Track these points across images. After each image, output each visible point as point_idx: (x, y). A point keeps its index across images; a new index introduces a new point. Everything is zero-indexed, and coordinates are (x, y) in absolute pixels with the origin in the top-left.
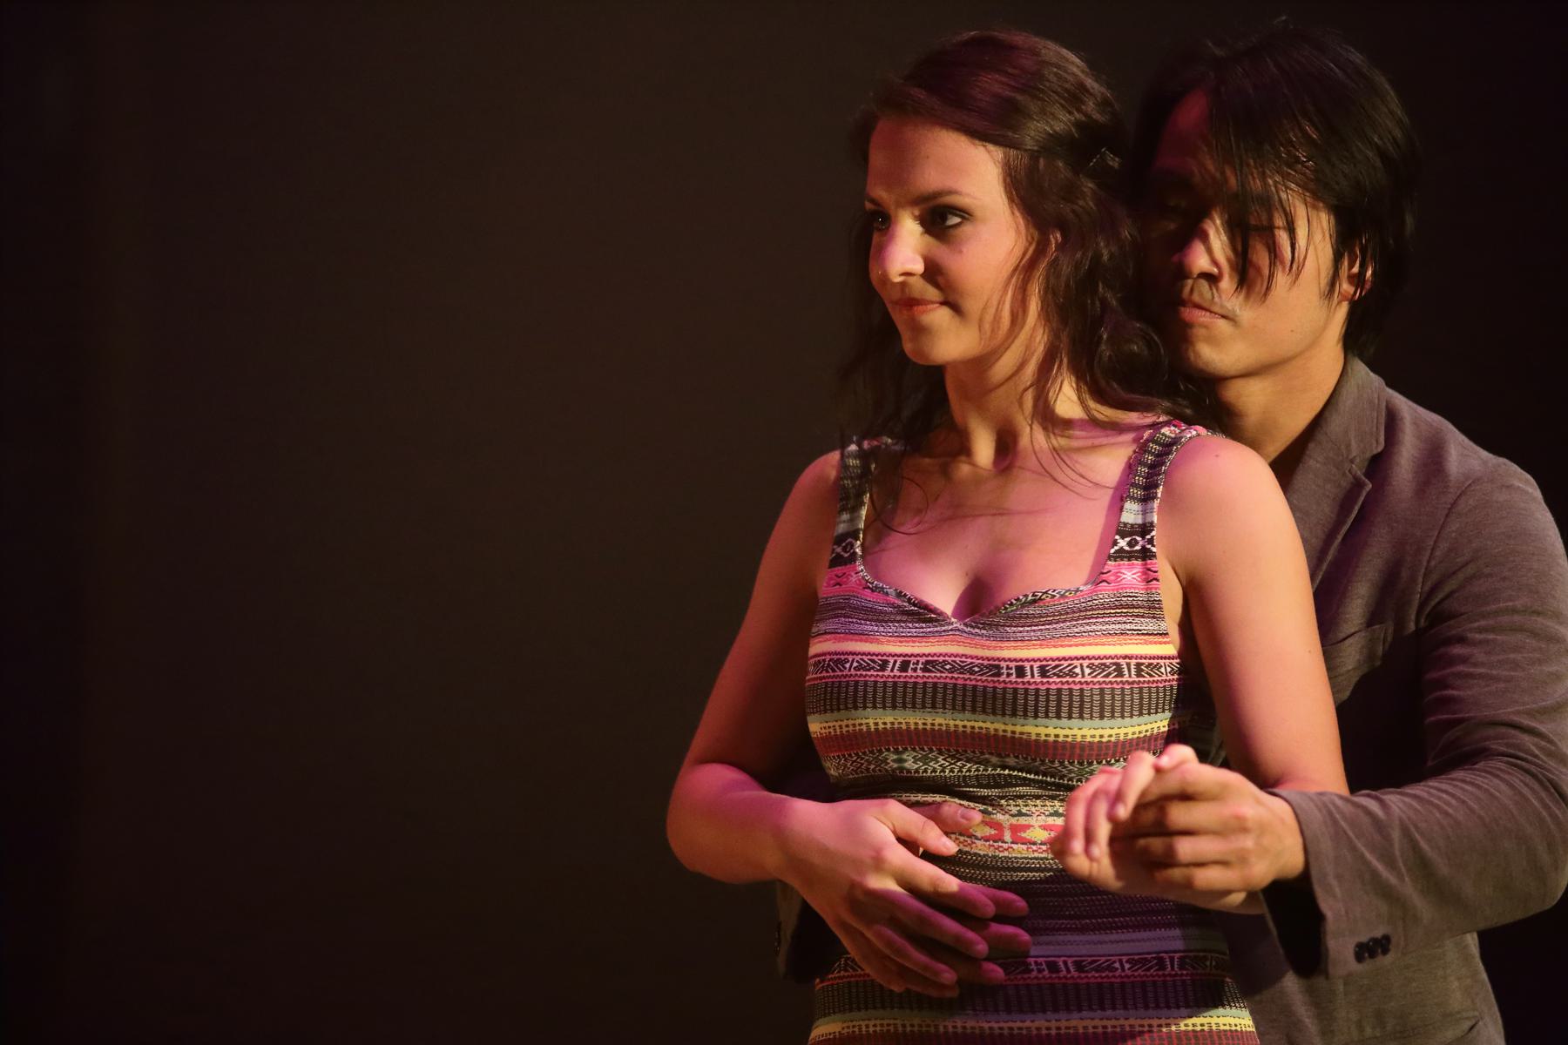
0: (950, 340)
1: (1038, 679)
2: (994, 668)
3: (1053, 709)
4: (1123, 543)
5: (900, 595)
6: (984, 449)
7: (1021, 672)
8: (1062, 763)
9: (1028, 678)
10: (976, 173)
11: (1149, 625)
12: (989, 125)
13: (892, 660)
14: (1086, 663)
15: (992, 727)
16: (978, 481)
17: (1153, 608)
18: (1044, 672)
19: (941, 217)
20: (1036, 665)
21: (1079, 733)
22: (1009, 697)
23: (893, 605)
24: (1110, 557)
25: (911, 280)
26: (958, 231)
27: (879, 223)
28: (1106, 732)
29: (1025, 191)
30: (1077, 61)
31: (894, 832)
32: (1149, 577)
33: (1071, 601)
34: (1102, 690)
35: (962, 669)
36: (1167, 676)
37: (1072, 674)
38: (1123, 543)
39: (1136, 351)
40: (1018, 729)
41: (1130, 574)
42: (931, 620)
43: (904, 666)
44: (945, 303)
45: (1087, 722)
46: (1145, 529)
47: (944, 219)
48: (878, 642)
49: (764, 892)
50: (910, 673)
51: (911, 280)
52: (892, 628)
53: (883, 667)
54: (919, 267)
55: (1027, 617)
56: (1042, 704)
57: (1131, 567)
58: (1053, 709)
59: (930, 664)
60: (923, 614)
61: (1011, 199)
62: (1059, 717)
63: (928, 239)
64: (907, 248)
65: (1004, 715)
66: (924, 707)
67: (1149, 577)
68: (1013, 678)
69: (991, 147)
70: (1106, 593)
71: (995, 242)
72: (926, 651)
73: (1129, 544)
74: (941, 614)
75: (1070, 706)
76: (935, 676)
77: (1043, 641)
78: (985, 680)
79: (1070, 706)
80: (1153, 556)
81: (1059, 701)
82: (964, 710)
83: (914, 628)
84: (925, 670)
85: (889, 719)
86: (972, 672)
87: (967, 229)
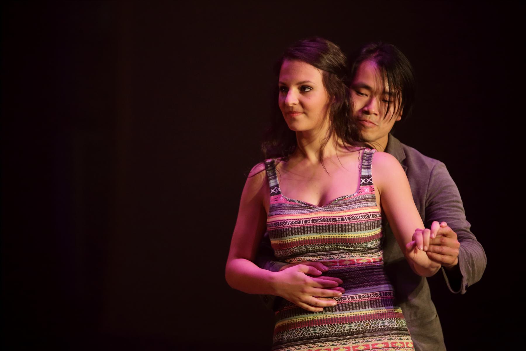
0: (302, 123)
1: (348, 221)
2: (335, 219)
3: (353, 229)
4: (363, 181)
5: (299, 202)
6: (313, 157)
7: (343, 219)
8: (355, 244)
9: (345, 221)
10: (314, 75)
11: (373, 203)
12: (315, 61)
13: (302, 220)
14: (360, 215)
15: (335, 236)
16: (313, 166)
17: (373, 199)
18: (349, 219)
19: (304, 88)
20: (347, 217)
21: (360, 235)
22: (340, 227)
23: (298, 205)
24: (361, 185)
25: (294, 106)
26: (308, 93)
27: (286, 89)
28: (367, 234)
29: (327, 82)
30: (336, 46)
31: (306, 274)
32: (372, 190)
33: (353, 199)
34: (354, 224)
35: (324, 221)
36: (378, 217)
37: (357, 219)
38: (363, 181)
39: (349, 129)
40: (343, 236)
41: (367, 189)
42: (311, 208)
43: (306, 222)
44: (304, 113)
45: (362, 232)
46: (277, 186)
47: (305, 89)
48: (296, 215)
49: (266, 298)
50: (308, 223)
51: (294, 106)
52: (300, 211)
53: (299, 222)
54: (297, 102)
55: (341, 204)
56: (350, 228)
57: (367, 187)
58: (353, 229)
59: (314, 220)
60: (308, 206)
61: (324, 85)
62: (355, 231)
63: (301, 95)
64: (293, 97)
65: (339, 232)
66: (314, 232)
67: (372, 190)
68: (341, 221)
69: (320, 70)
70: (362, 196)
71: (318, 97)
72: (312, 217)
73: (365, 181)
74: (314, 206)
75: (358, 228)
76: (315, 224)
77: (347, 210)
78: (333, 223)
79: (358, 228)
80: (372, 184)
81: (355, 226)
82: (326, 232)
83: (306, 211)
84: (312, 222)
85: (303, 237)
86: (328, 221)
87: (312, 92)
